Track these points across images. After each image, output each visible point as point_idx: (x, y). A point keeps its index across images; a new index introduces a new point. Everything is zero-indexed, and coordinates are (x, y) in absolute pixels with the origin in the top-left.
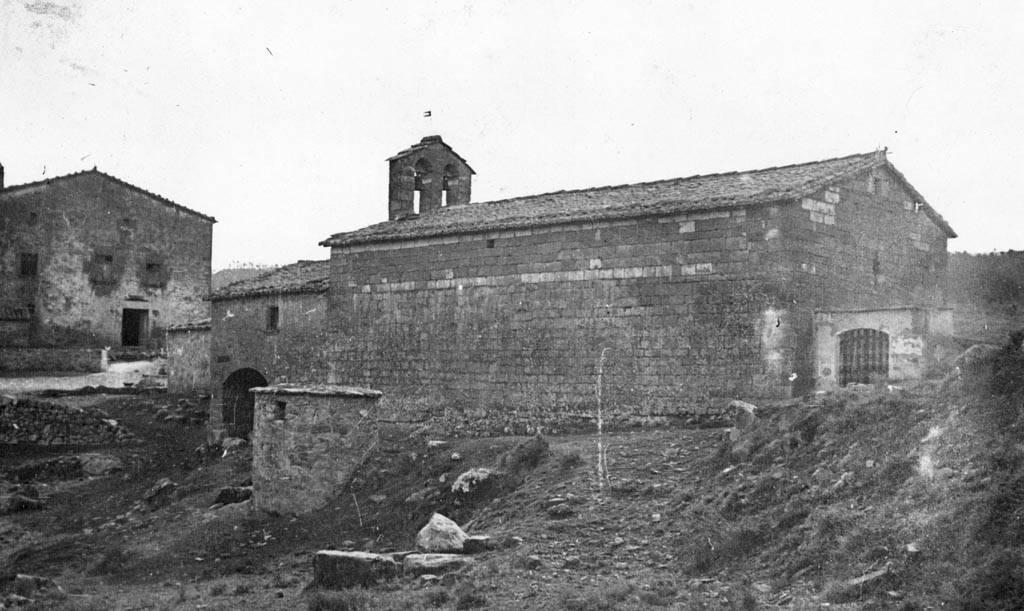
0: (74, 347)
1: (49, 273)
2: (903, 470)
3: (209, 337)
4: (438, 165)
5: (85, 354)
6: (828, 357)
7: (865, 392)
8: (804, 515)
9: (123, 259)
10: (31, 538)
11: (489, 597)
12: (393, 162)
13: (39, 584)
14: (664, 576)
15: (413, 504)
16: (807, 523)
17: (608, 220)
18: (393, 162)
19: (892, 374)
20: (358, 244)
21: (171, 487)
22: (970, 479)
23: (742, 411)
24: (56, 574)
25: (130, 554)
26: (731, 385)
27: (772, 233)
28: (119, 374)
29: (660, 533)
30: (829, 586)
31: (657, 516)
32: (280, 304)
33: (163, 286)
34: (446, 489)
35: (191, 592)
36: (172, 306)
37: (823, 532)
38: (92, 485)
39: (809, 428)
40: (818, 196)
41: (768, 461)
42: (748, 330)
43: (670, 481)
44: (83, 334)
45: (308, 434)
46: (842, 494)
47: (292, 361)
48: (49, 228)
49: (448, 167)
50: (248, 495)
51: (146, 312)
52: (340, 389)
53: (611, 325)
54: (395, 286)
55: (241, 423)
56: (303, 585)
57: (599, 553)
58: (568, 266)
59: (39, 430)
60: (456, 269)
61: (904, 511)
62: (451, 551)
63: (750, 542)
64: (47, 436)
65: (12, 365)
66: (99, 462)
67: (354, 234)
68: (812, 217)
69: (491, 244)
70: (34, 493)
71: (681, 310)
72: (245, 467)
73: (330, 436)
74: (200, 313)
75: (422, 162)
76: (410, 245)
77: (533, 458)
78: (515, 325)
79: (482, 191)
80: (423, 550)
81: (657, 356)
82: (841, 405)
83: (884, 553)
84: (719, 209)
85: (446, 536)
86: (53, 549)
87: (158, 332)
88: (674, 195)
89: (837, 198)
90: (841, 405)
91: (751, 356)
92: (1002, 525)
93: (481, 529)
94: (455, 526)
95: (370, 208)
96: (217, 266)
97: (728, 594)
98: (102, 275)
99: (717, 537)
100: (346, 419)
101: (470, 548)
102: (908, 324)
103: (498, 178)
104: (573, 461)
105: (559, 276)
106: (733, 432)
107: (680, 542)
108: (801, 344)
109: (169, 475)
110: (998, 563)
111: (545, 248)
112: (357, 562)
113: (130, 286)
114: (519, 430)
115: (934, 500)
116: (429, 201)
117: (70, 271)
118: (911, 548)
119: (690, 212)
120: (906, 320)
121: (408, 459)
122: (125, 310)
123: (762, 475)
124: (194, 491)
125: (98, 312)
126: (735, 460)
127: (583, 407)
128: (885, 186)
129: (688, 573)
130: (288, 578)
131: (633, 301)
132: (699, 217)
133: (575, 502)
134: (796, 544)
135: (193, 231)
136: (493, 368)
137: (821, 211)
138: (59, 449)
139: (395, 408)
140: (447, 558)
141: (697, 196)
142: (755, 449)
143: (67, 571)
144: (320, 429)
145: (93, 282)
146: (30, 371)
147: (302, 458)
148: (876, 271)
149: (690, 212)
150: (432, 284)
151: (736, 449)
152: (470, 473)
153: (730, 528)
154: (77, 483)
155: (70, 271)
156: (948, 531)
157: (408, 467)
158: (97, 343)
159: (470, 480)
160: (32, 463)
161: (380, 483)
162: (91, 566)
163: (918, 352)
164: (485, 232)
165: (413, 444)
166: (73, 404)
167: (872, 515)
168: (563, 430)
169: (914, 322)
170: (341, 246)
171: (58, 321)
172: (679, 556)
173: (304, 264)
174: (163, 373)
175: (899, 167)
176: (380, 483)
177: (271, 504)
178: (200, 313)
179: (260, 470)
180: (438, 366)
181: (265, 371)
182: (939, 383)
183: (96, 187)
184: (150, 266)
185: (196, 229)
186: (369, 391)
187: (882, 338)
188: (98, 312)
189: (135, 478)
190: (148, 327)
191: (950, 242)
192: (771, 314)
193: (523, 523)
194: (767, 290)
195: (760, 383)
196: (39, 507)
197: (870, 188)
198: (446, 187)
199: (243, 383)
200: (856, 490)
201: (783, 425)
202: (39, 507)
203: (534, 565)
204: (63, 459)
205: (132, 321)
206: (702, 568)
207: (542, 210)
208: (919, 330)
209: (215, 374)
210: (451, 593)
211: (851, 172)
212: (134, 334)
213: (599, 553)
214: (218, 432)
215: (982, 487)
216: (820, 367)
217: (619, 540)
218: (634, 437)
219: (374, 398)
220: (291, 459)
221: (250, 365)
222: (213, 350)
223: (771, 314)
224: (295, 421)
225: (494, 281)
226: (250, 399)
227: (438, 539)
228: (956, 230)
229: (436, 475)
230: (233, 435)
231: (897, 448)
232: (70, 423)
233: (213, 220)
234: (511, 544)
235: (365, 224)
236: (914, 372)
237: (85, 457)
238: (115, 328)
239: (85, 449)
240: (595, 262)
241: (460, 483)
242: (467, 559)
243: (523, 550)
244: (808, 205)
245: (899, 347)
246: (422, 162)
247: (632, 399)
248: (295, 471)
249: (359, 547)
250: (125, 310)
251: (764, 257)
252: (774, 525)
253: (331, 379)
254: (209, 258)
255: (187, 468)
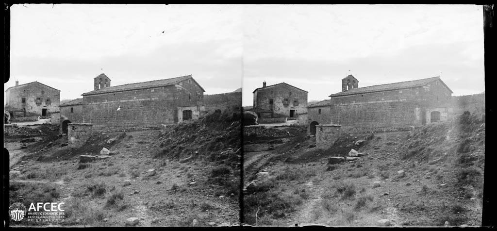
0: (280, 118)
1: (275, 103)
2: (443, 139)
3: (307, 115)
4: (104, 80)
5: (35, 118)
6: (428, 117)
7: (436, 124)
8: (424, 148)
9: (290, 100)
10: (272, 155)
11: (363, 165)
12: (95, 79)
13: (26, 163)
14: (397, 160)
15: (347, 147)
16: (425, 149)
17: (386, 91)
18: (95, 79)
19: (441, 120)
20: (88, 95)
21: (300, 145)
22: (456, 140)
23: (412, 128)
24: (278, 162)
25: (44, 157)
26: (161, 122)
27: (417, 93)
28: (289, 123)
29: (148, 150)
30: (181, 160)
31: (396, 149)
32: (321, 108)
33: (298, 105)
34: (106, 143)
35: (56, 164)
36: (52, 108)
37: (179, 149)
38: (284, 145)
39: (425, 131)
40: (426, 85)
41: (169, 136)
42: (413, 112)
43: (149, 141)
44: (282, 115)
45: (327, 134)
46: (182, 142)
47: (323, 120)
48: (275, 94)
49: (106, 80)
50: (315, 146)
51: (294, 110)
52: (85, 124)
53: (139, 110)
54: (344, 104)
55: (314, 131)
56: (326, 164)
57: (385, 156)
58: (378, 100)
59: (274, 134)
60: (355, 101)
61: (444, 146)
62: (107, 155)
63: (414, 153)
64: (275, 135)
65: (20, 120)
66: (285, 140)
67: (335, 94)
68: (177, 88)
69: (362, 96)
70: (273, 147)
71: (152, 107)
72: (315, 140)
73: (83, 133)
74: (305, 110)
75: (101, 79)
76: (98, 95)
77: (371, 138)
78: (367, 112)
79: (112, 85)
80: (101, 155)
81: (147, 116)
82: (431, 126)
83: (440, 155)
84: (407, 88)
85: (354, 153)
86: (277, 157)
87: (297, 114)
88: (398, 86)
89: (430, 86)
90: (431, 126)
91: (414, 117)
92: (463, 149)
93: (361, 152)
94: (107, 150)
95: (338, 89)
96: (61, 100)
97: (410, 164)
98: (38, 101)
99: (407, 152)
100: (86, 130)
101: (359, 156)
102: (444, 110)
103: (364, 83)
104: (379, 138)
105: (128, 101)
106: (410, 132)
107: (151, 152)
108: (423, 114)
109: (299, 142)
110: (462, 157)
111: (373, 96)
112: (337, 159)
113: (291, 105)
114: (368, 132)
115: (449, 145)
116: (102, 86)
117: (279, 103)
118: (445, 154)
119: (153, 88)
120: (196, 108)
121: (98, 137)
122: (43, 109)
123: (167, 139)
124: (305, 145)
125: (285, 111)
126: (411, 137)
127: (381, 128)
128: (191, 82)
129: (153, 158)
130: (323, 162)
131: (143, 105)
132: (155, 89)
133: (379, 146)
134: (423, 153)
135: (56, 93)
136: (363, 120)
137: (427, 88)
138: (278, 138)
139: (344, 129)
140: (355, 158)
141: (154, 85)
142: (415, 135)
143: (280, 162)
144: (81, 131)
145: (36, 103)
146: (24, 121)
147: (326, 139)
148: (438, 100)
149: (153, 88)
150: (351, 104)
151: (411, 135)
152: (359, 141)
153: (410, 151)
154: (34, 143)
155: (279, 103)
156: (452, 151)
157: (98, 138)
158: (285, 117)
159: (359, 142)
160: (272, 140)
161: (93, 142)
162: (284, 161)
163: (198, 114)
164: (361, 93)
165: (348, 135)
166: (280, 129)
167: (437, 148)
168: (129, 131)
169: (445, 109)
170: (85, 95)
171: (277, 113)
172: (151, 155)
173: (78, 99)
174: (298, 122)
175: (442, 80)
176: (93, 142)
177: (320, 148)
178: (305, 110)
179: (318, 141)
180: (352, 120)
181: (318, 122)
182: (450, 122)
183: (284, 86)
184: (47, 100)
185: (304, 94)
186: (339, 125)
187: (191, 111)
188: (285, 111)
189: (45, 142)
190: (295, 113)
191: (204, 93)
192: (417, 109)
193: (121, 149)
194: (416, 104)
195: (415, 122)
196: (274, 149)
197: (188, 82)
198: (100, 83)
199: (314, 125)
200: (186, 141)
201: (420, 130)
202: (274, 149)
203: (372, 159)
204: (278, 140)
205: (292, 112)
206: (404, 159)
207: (372, 89)
208: (198, 110)
209: (61, 121)
210: (107, 163)
211: (184, 79)
212: (45, 113)
213: (385, 156)
214: (309, 134)
215: (459, 142)
216: (179, 118)
217: (140, 152)
218: (143, 132)
219: (340, 127)
220: (323, 140)
221: (315, 120)
222: (308, 117)
223: (417, 109)
224: (324, 132)
225: (363, 103)
226: (315, 127)
227: (104, 153)
228: (453, 92)
229: (352, 141)
230: (64, 133)
231: (442, 134)
232: (280, 133)
233: (308, 92)
234: (119, 153)
235: (337, 92)
236: (197, 118)
237: (283, 139)
238: (288, 114)
239: (283, 137)
240: (135, 98)
241: (357, 143)
242: (358, 158)
243: (370, 156)
244: (424, 87)
245: (194, 113)
246: (349, 80)
247: (143, 124)
248: (325, 141)
249: (337, 156)
250: (43, 109)
251: (416, 97)
252: (419, 150)
253: (331, 123)
254: (59, 98)
255: (55, 140)
